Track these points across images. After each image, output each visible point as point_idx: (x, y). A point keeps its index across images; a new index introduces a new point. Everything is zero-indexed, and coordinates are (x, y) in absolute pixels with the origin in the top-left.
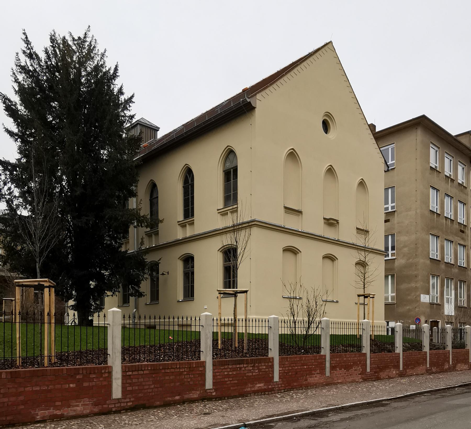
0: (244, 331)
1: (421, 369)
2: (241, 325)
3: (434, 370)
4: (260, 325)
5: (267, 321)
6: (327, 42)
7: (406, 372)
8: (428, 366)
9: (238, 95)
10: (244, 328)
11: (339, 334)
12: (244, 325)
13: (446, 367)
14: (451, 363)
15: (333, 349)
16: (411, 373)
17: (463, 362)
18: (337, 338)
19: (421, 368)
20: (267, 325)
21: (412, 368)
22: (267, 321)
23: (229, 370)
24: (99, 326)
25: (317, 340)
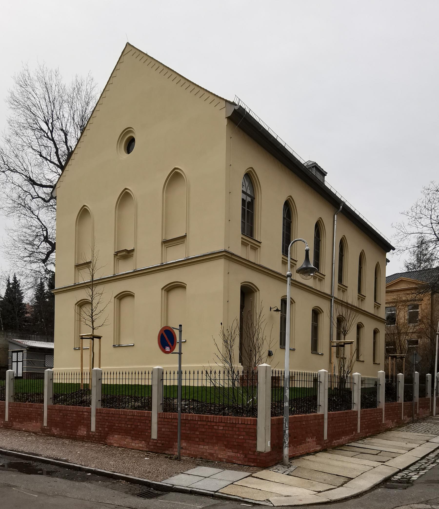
0: (80, 382)
1: (32, 426)
2: (86, 378)
3: (55, 431)
4: (124, 378)
5: (150, 373)
6: (330, 182)
7: (12, 425)
8: (45, 424)
9: (354, 212)
10: (80, 380)
11: (298, 387)
12: (80, 378)
13: (83, 432)
14: (93, 428)
15: (55, 398)
16: (19, 427)
17: (126, 432)
18: (109, 389)
19: (34, 424)
20: (88, 378)
21: (21, 422)
22: (150, 373)
23: (207, 427)
24: (163, 380)
25: (42, 388)
